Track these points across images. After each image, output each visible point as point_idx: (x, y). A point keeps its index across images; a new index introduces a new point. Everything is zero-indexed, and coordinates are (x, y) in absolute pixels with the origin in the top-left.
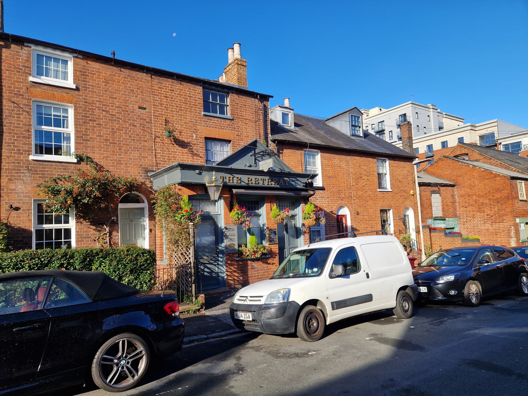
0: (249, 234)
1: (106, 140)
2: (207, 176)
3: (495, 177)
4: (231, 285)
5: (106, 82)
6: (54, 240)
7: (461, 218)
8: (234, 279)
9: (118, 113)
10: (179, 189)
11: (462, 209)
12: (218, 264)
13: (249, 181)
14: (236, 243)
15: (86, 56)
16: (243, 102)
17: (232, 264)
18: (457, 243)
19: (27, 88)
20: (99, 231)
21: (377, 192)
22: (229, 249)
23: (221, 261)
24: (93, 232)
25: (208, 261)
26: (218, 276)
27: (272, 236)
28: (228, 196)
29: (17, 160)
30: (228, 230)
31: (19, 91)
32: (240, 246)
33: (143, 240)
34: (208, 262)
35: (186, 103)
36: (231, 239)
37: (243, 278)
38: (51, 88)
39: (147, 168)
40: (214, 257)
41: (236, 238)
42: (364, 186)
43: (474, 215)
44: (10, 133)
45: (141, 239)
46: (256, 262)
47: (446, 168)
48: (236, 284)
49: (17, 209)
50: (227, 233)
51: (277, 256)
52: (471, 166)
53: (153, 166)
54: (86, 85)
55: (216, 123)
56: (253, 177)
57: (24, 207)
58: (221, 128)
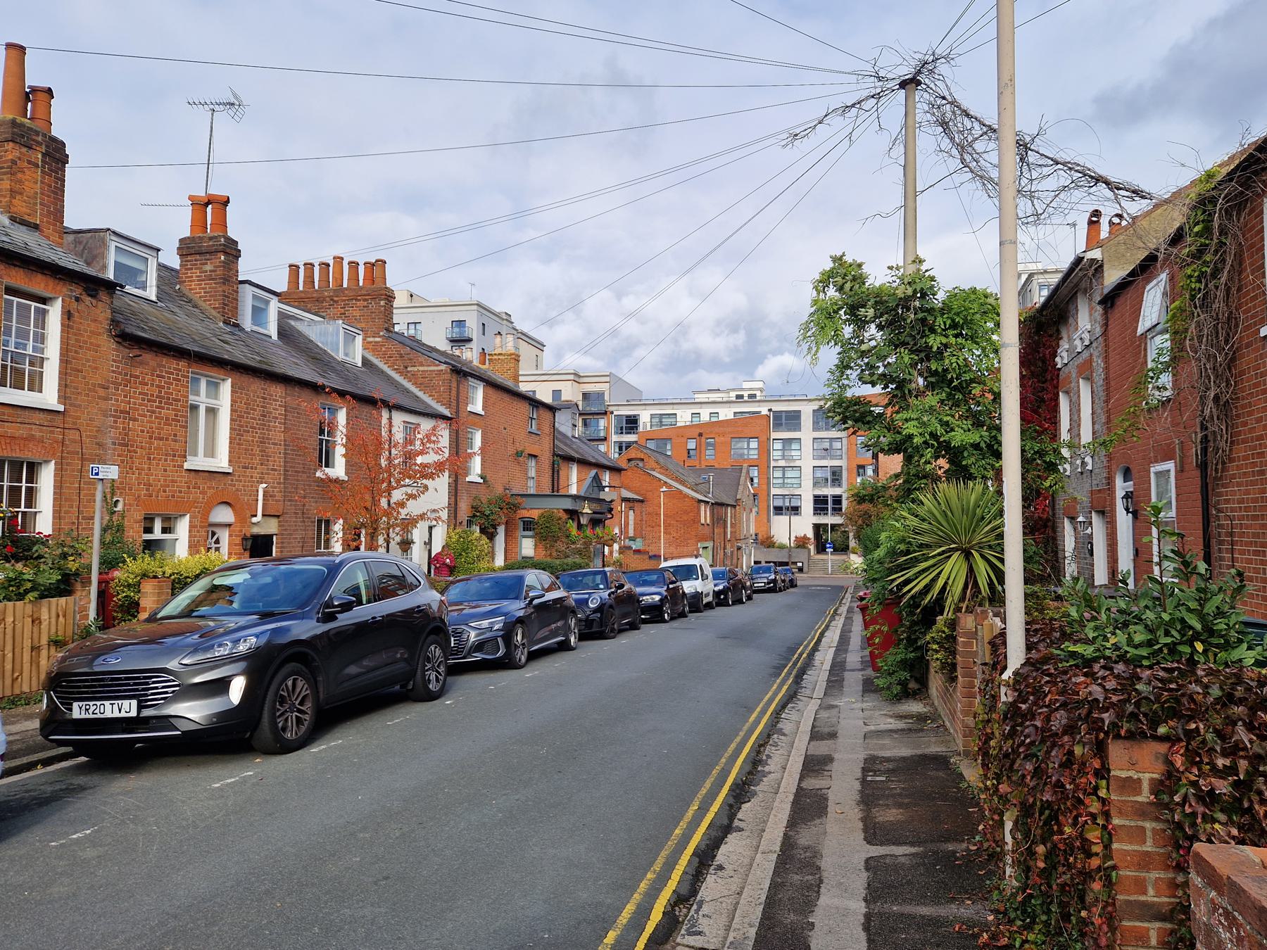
6: (32, 332)
11: (648, 529)
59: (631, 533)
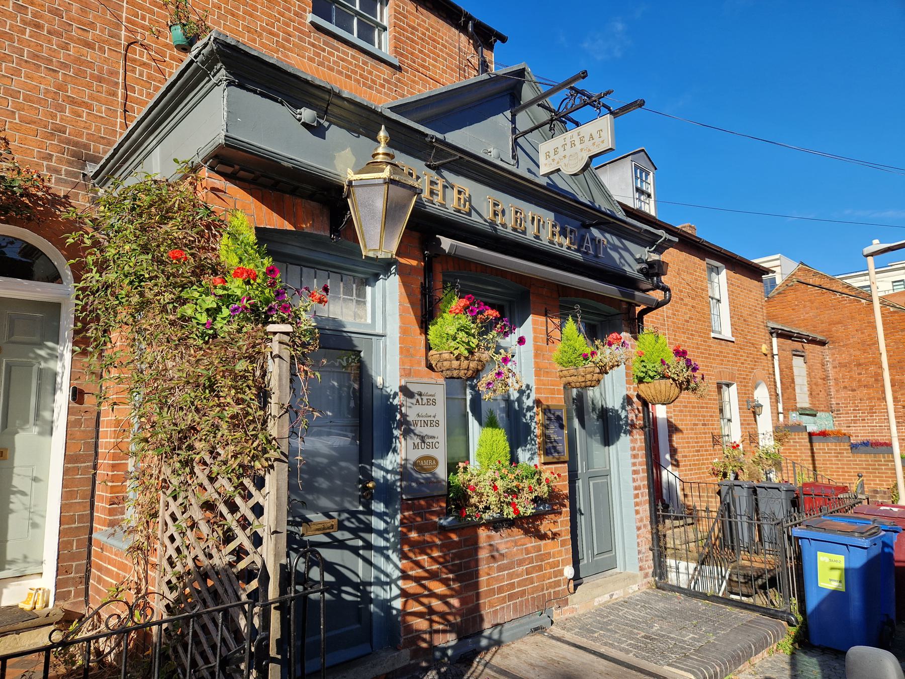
0: (476, 423)
2: (348, 150)
4: (417, 636)
7: (843, 414)
8: (431, 611)
10: (214, 190)
11: (843, 394)
12: (369, 546)
13: (495, 214)
14: (441, 454)
16: (428, 30)
17: (425, 542)
18: (886, 469)
21: (709, 338)
22: (416, 480)
23: (380, 533)
25: (328, 535)
26: (366, 598)
27: (553, 432)
28: (414, 263)
30: (414, 401)
32: (452, 468)
33: (41, 433)
34: (327, 540)
36: (423, 439)
37: (463, 602)
39: (86, 146)
40: (354, 514)
41: (440, 432)
42: (687, 321)
43: (871, 408)
45: (36, 430)
46: (504, 532)
47: (805, 307)
48: (437, 631)
50: (412, 411)
51: (565, 506)
55: (351, 63)
56: (509, 203)
58: (364, 84)
59: (803, 400)
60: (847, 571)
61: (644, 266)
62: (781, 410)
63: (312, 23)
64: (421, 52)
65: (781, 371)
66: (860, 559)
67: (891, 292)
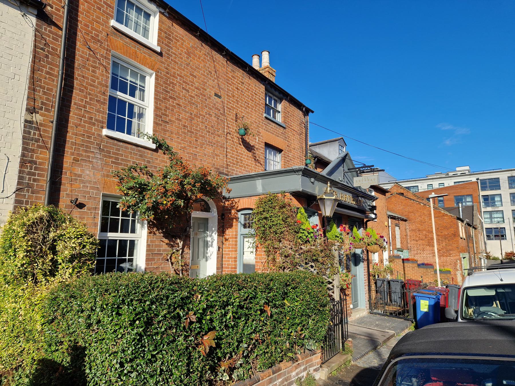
1: (184, 126)
3: (443, 216)
5: (188, 54)
9: (196, 95)
11: (413, 242)
15: (172, 15)
19: (108, 35)
20: (172, 246)
24: (165, 247)
29: (87, 132)
31: (98, 36)
35: (253, 101)
38: (133, 43)
44: (82, 91)
47: (399, 204)
49: (81, 206)
52: (422, 204)
53: (223, 167)
54: (169, 51)
57: (90, 204)
59: (399, 245)
60: (429, 306)
61: (370, 207)
62: (391, 249)
63: (265, 117)
64: (290, 120)
65: (392, 233)
66: (433, 302)
67: (427, 190)
